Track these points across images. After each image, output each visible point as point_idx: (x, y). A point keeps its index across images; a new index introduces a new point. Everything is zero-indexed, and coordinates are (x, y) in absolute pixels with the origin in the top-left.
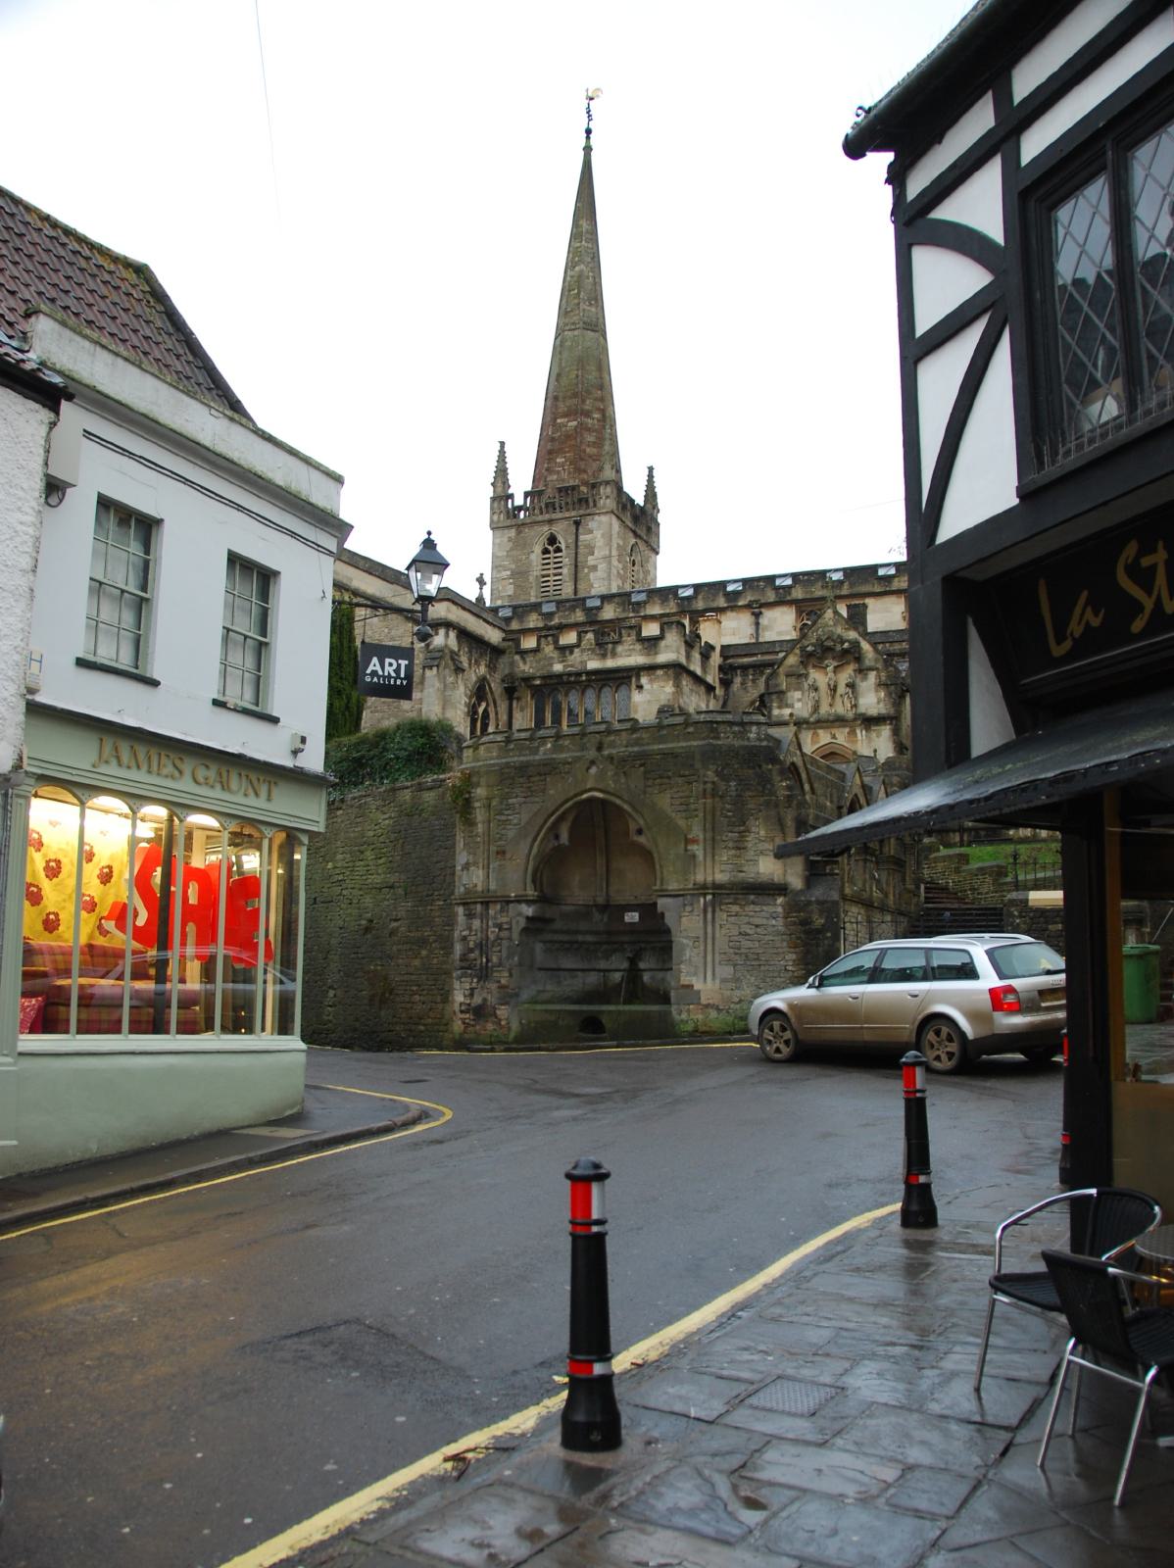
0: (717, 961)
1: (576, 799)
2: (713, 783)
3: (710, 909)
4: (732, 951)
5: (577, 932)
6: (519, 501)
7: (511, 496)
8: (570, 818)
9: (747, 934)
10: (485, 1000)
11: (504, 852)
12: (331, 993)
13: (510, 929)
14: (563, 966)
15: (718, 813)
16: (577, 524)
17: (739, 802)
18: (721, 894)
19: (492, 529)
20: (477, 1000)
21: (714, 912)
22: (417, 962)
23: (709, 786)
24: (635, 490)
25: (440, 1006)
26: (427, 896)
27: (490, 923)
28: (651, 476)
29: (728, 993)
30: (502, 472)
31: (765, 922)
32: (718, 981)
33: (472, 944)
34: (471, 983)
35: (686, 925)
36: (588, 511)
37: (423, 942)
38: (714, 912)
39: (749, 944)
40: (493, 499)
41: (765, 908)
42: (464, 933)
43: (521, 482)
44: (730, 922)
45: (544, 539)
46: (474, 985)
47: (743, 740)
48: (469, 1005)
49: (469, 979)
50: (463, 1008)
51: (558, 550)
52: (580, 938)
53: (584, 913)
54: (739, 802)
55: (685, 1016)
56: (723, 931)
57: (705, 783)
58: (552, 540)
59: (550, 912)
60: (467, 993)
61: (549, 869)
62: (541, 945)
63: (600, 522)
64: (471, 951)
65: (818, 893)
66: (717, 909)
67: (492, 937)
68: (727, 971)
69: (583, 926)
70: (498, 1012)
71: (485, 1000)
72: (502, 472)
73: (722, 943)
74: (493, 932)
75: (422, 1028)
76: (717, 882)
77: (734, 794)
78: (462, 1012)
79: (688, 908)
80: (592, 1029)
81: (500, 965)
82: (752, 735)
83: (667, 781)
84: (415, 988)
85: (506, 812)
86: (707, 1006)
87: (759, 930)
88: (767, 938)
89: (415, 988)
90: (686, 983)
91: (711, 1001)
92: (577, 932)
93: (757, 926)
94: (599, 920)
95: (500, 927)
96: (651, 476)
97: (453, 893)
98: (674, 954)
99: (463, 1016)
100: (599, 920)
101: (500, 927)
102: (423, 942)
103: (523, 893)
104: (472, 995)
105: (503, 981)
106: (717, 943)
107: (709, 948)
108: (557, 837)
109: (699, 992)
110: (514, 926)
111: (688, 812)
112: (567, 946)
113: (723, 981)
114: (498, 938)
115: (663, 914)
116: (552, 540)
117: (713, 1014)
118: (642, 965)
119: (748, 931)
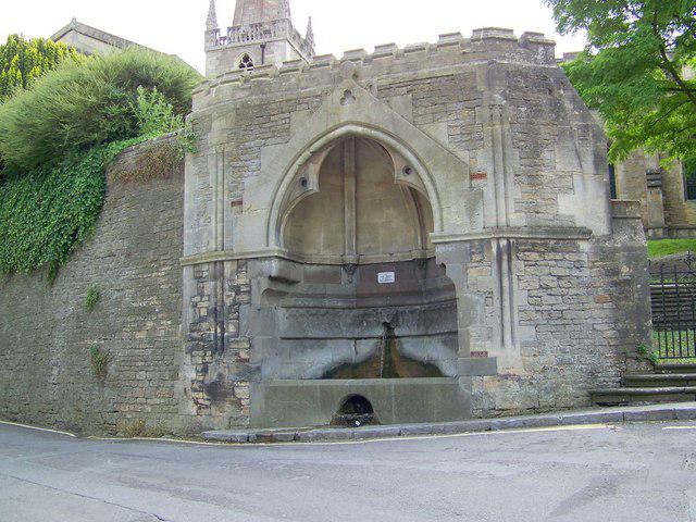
0: (516, 322)
1: (331, 135)
2: (501, 107)
3: (505, 257)
4: (532, 308)
5: (323, 296)
6: (224, 33)
7: (217, 31)
8: (324, 154)
9: (548, 288)
10: (220, 376)
11: (240, 203)
12: (55, 372)
13: (249, 292)
14: (310, 335)
15: (509, 142)
16: (263, 47)
17: (530, 132)
18: (512, 248)
19: (207, 52)
20: (212, 376)
21: (509, 260)
22: (142, 335)
23: (497, 111)
24: (301, 27)
25: (169, 383)
26: (153, 261)
27: (226, 286)
28: (310, 22)
29: (531, 359)
30: (212, 15)
31: (567, 272)
32: (518, 345)
33: (203, 312)
34: (203, 357)
35: (474, 281)
36: (272, 39)
37: (148, 312)
38: (509, 260)
39: (552, 300)
40: (207, 33)
41: (567, 256)
42: (195, 299)
43: (225, 21)
44: (526, 278)
45: (242, 55)
46: (207, 359)
47: (528, 58)
48: (203, 382)
49: (201, 353)
50: (196, 386)
51: (251, 65)
52: (327, 303)
53: (330, 274)
54: (530, 132)
55: (484, 388)
56: (522, 284)
57: (492, 107)
58: (246, 59)
59: (295, 272)
60: (200, 368)
61: (298, 212)
62: (284, 310)
63: (278, 46)
64: (202, 319)
65: (622, 239)
66: (514, 257)
67: (228, 302)
68: (526, 333)
69: (330, 288)
70: (237, 391)
71: (220, 376)
72: (212, 15)
73: (520, 298)
74: (229, 296)
75: (149, 409)
76: (512, 224)
77: (524, 120)
78: (195, 390)
79: (476, 257)
80: (357, 409)
81: (237, 334)
82: (539, 57)
83: (441, 107)
84: (140, 364)
85: (244, 157)
86: (506, 377)
87: (562, 283)
88: (572, 292)
89: (140, 364)
90: (477, 349)
91: (511, 372)
92: (323, 296)
93: (559, 278)
94: (347, 284)
95: (237, 290)
96: (310, 22)
97: (181, 255)
98: (460, 314)
99: (195, 395)
100: (347, 284)
101: (237, 290)
102: (148, 312)
103: (266, 248)
104: (205, 370)
105: (243, 355)
106: (515, 299)
107: (507, 304)
108: (304, 182)
109: (494, 360)
110: (254, 287)
111: (471, 139)
112: (313, 311)
113: (525, 345)
114: (236, 303)
115: (443, 265)
116: (246, 59)
117: (514, 386)
118: (397, 332)
119: (551, 285)
